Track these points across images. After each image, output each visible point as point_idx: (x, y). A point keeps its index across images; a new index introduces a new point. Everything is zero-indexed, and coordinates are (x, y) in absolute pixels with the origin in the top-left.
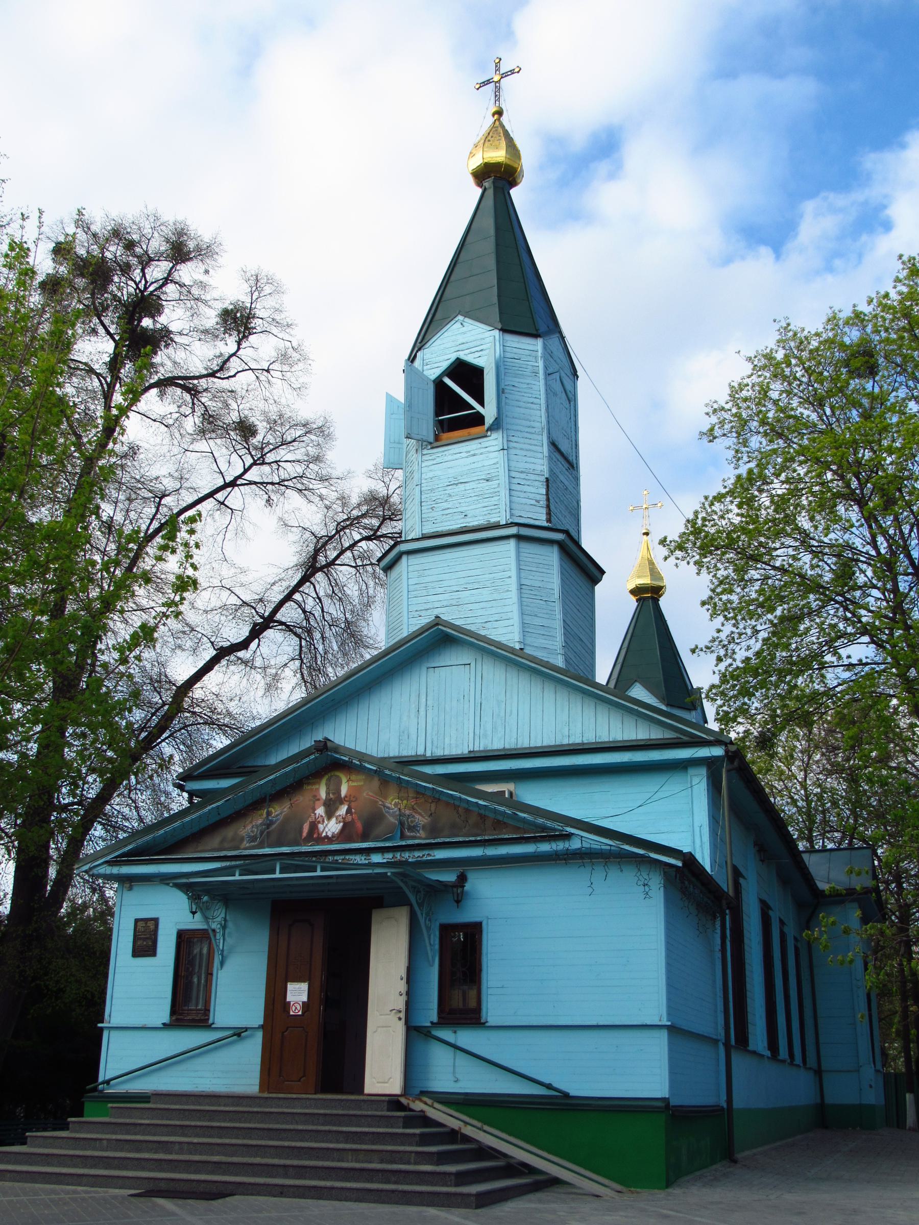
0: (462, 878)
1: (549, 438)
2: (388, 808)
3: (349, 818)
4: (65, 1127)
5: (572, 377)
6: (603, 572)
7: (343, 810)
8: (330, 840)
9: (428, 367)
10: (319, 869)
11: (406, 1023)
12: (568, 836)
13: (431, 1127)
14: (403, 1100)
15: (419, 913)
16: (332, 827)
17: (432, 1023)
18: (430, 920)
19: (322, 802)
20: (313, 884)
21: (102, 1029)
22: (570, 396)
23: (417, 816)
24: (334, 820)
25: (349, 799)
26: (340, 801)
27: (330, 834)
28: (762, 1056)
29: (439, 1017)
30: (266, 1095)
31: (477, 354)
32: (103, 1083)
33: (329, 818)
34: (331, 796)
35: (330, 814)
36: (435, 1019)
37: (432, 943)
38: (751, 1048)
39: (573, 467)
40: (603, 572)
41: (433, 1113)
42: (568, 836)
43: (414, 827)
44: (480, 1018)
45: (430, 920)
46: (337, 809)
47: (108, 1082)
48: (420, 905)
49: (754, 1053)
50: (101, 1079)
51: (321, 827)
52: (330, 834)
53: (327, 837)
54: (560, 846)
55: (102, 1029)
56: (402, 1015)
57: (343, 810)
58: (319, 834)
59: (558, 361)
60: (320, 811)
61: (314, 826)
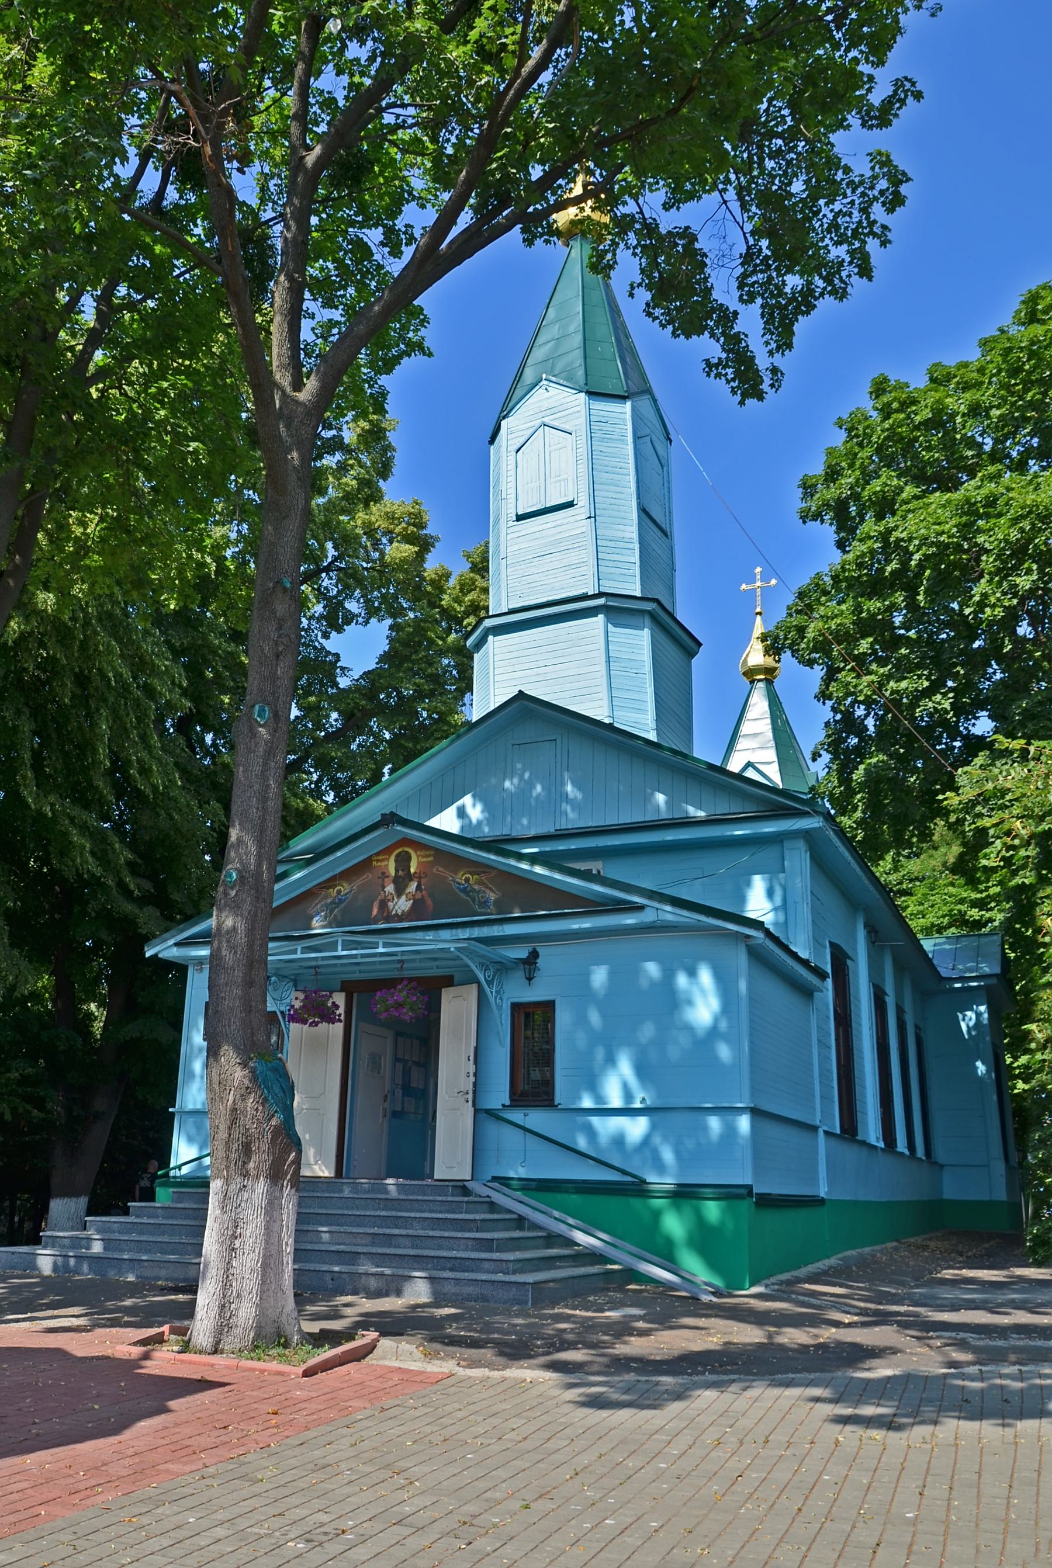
0: (534, 955)
1: (639, 504)
2: (459, 884)
3: (419, 895)
4: (126, 1212)
5: (664, 441)
6: (700, 645)
7: (413, 887)
8: (400, 918)
9: (513, 435)
10: (381, 944)
11: (474, 1105)
12: (641, 908)
13: (499, 1213)
14: (470, 1185)
15: (487, 989)
16: (403, 905)
17: (503, 1105)
18: (501, 999)
19: (391, 879)
20: (381, 963)
21: (173, 1114)
22: (663, 462)
23: (488, 892)
24: (404, 897)
25: (418, 876)
26: (410, 877)
27: (399, 912)
28: (875, 1147)
29: (512, 1100)
30: (402, 1197)
31: (564, 420)
32: (174, 1168)
33: (399, 896)
34: (401, 873)
35: (400, 891)
36: (508, 1102)
37: (503, 1023)
38: (859, 1138)
39: (666, 535)
40: (700, 645)
41: (498, 1198)
42: (641, 908)
43: (485, 902)
44: (553, 1100)
45: (501, 999)
46: (406, 886)
47: (179, 1167)
48: (490, 983)
49: (864, 1144)
50: (172, 1166)
51: (391, 904)
52: (399, 912)
53: (396, 914)
54: (630, 920)
55: (173, 1114)
56: (470, 1097)
57: (413, 887)
58: (389, 912)
59: (649, 424)
60: (390, 888)
61: (383, 904)
